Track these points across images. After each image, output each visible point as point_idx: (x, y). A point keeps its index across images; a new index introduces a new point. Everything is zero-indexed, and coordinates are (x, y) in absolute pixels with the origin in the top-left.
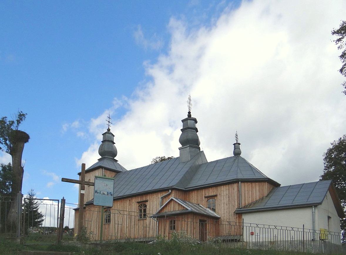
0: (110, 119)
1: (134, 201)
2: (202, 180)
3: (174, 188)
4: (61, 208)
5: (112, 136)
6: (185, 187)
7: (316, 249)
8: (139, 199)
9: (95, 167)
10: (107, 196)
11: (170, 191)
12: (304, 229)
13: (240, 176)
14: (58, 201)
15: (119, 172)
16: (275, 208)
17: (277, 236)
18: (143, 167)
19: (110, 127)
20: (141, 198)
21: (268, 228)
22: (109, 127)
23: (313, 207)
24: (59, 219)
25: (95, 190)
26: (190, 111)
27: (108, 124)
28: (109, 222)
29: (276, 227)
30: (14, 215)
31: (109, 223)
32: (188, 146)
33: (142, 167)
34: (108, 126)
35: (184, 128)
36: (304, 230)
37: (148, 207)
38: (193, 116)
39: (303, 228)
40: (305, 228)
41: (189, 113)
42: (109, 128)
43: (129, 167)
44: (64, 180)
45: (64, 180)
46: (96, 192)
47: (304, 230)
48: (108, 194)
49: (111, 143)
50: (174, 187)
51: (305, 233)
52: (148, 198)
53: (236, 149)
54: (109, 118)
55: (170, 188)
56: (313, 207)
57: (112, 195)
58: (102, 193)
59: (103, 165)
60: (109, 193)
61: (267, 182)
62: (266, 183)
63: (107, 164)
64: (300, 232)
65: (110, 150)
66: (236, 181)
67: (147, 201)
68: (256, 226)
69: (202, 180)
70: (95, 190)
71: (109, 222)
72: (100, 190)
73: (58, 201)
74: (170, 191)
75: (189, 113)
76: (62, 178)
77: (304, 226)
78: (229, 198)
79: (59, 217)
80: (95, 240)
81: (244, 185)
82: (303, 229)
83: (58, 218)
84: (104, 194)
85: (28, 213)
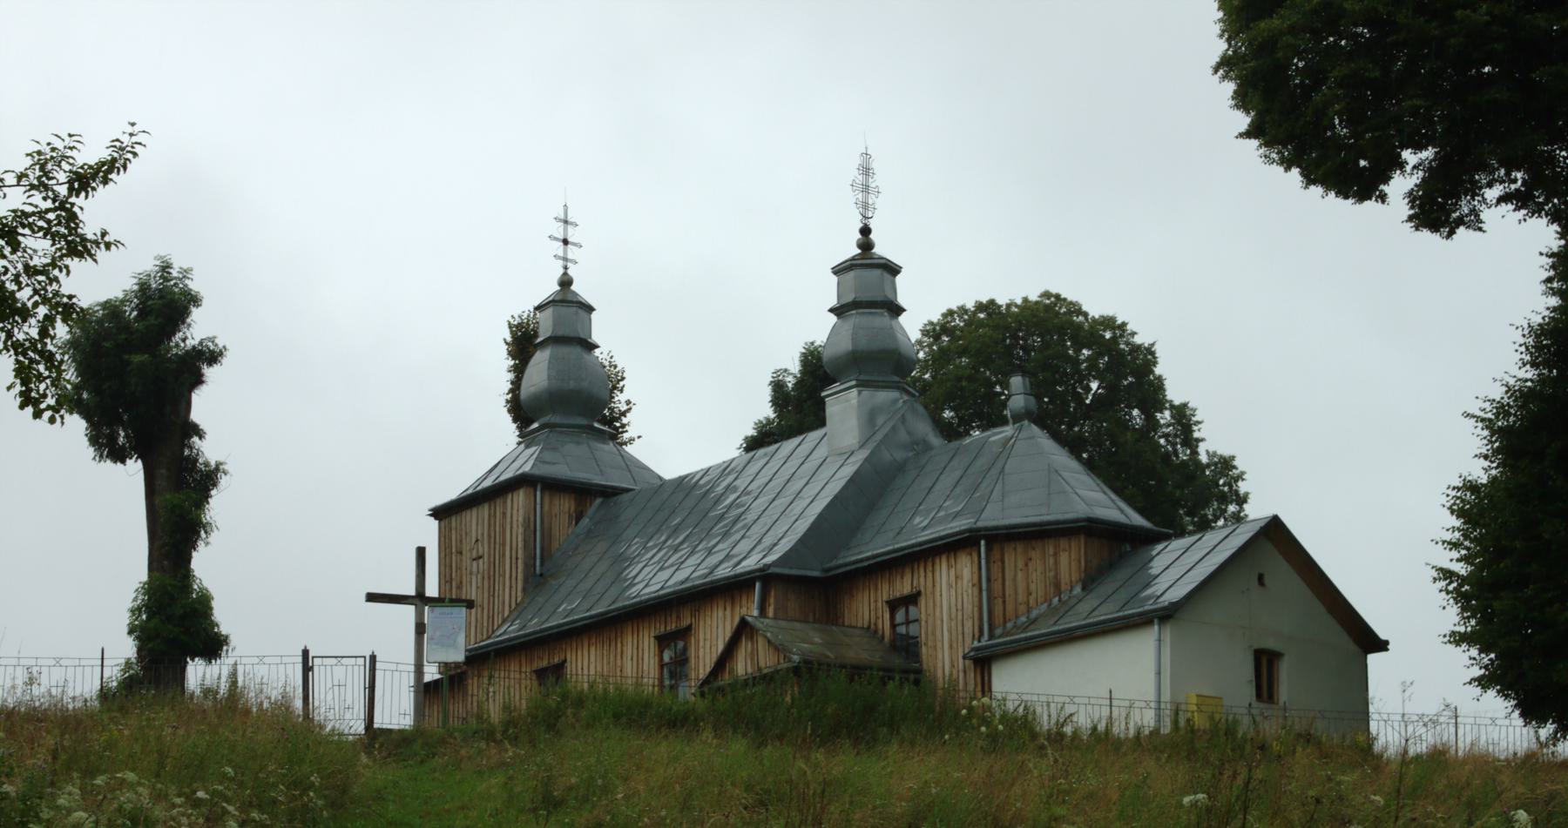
0: (561, 254)
2: (294, 691)
4: (370, 670)
5: (580, 311)
7: (512, 690)
14: (365, 657)
16: (1003, 647)
18: (709, 469)
19: (569, 265)
20: (949, 567)
22: (566, 268)
23: (1156, 621)
24: (367, 690)
26: (866, 225)
27: (561, 254)
29: (1148, 705)
32: (854, 383)
33: (680, 477)
34: (561, 263)
35: (844, 301)
36: (1111, 702)
38: (881, 249)
39: (1108, 697)
41: (865, 231)
42: (565, 274)
43: (669, 469)
44: (372, 597)
45: (372, 597)
47: (1111, 702)
49: (577, 351)
53: (1013, 397)
54: (566, 222)
55: (757, 574)
56: (1156, 621)
63: (574, 462)
65: (572, 385)
69: (294, 691)
73: (365, 657)
75: (865, 231)
77: (1111, 692)
78: (342, 688)
79: (367, 686)
83: (365, 688)
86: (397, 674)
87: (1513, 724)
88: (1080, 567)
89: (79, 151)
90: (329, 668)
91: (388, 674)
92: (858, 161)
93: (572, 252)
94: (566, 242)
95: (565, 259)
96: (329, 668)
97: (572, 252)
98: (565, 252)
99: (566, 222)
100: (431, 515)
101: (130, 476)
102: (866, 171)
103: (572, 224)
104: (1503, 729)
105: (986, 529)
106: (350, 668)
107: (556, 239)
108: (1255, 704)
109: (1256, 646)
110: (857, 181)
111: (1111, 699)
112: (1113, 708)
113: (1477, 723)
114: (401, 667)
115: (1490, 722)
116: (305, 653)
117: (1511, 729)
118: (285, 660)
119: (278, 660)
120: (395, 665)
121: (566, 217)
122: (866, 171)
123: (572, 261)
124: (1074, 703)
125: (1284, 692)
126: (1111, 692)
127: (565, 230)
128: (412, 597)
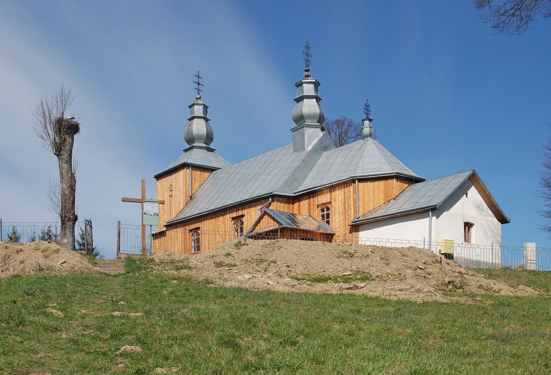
1: (229, 216)
3: (274, 194)
6: (294, 192)
8: (234, 215)
9: (171, 168)
10: (154, 216)
11: (270, 199)
12: (425, 242)
13: (360, 173)
15: (216, 170)
17: (545, 257)
21: (464, 247)
25: (144, 212)
28: (199, 250)
30: (465, 301)
31: (199, 252)
36: (424, 242)
37: (245, 224)
40: (425, 241)
44: (124, 200)
45: (124, 200)
46: (144, 214)
48: (154, 215)
50: (275, 193)
51: (494, 250)
52: (245, 212)
54: (199, 77)
57: (158, 215)
58: (149, 214)
59: (190, 161)
60: (155, 214)
61: (395, 179)
62: (394, 179)
64: (488, 250)
66: (353, 181)
67: (243, 216)
68: (386, 241)
70: (144, 212)
71: (199, 250)
72: (148, 212)
74: (270, 199)
76: (141, 179)
77: (424, 238)
80: (269, 295)
81: (282, 199)
82: (424, 241)
84: (151, 215)
85: (85, 242)
86: (466, 248)
87: (466, 247)
90: (474, 249)
94: (199, 84)
96: (474, 249)
97: (201, 88)
98: (198, 87)
99: (199, 77)
100: (154, 177)
101: (142, 203)
102: (307, 48)
103: (200, 77)
104: (482, 250)
107: (196, 83)
108: (464, 243)
109: (465, 221)
110: (304, 52)
111: (424, 241)
112: (493, 249)
113: (466, 247)
115: (387, 241)
116: (119, 222)
117: (485, 250)
118: (131, 227)
120: (531, 262)
121: (199, 75)
122: (307, 48)
123: (201, 90)
124: (479, 248)
125: (473, 240)
126: (424, 238)
127: (199, 81)
128: (141, 199)
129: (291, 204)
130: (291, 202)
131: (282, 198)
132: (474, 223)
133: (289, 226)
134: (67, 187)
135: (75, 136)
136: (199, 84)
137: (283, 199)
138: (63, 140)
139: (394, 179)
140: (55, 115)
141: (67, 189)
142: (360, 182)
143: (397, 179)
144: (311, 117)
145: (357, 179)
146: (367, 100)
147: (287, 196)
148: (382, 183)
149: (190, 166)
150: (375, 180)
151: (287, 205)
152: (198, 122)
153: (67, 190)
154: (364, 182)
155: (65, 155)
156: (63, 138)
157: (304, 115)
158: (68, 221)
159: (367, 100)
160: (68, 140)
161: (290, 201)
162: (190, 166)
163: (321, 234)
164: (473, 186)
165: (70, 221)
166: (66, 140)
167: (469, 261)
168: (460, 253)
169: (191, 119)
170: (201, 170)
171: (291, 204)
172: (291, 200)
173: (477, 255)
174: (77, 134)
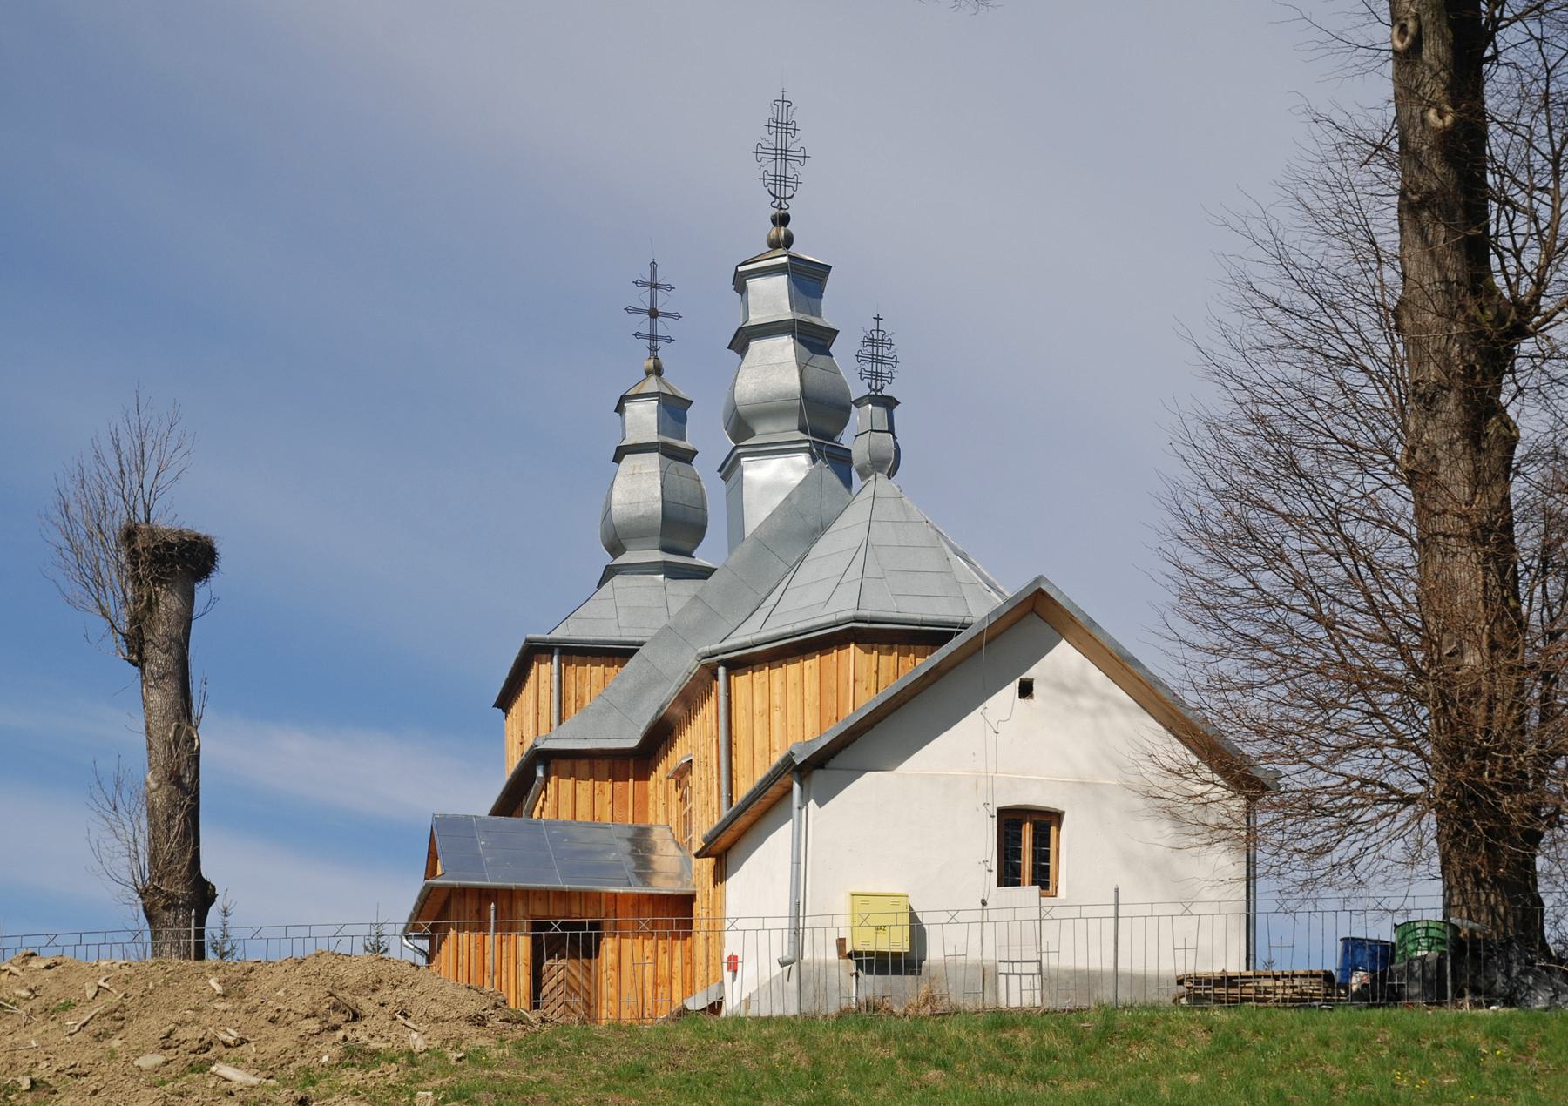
36: (1117, 909)
47: (1117, 909)
54: (654, 286)
61: (856, 643)
74: (540, 773)
77: (1117, 891)
86: (1152, 922)
88: (1161, 684)
89: (629, 310)
90: (1165, 921)
91: (1139, 922)
92: (767, 113)
93: (663, 326)
94: (654, 314)
95: (653, 337)
96: (1165, 921)
97: (663, 326)
99: (654, 286)
102: (783, 126)
105: (559, 641)
106: (1206, 920)
114: (769, 924)
117: (1152, 922)
118: (1086, 912)
119: (757, 924)
122: (783, 126)
123: (663, 339)
126: (1117, 891)
129: (631, 780)
130: (631, 774)
131: (586, 761)
132: (1060, 808)
133: (1027, 869)
134: (159, 781)
135: (202, 592)
136: (654, 314)
137: (590, 763)
138: (142, 605)
139: (852, 646)
140: (116, 522)
141: (159, 787)
142: (739, 671)
143: (866, 646)
144: (771, 411)
145: (722, 663)
146: (878, 319)
147: (602, 750)
148: (811, 664)
149: (557, 651)
150: (789, 660)
151: (608, 786)
152: (634, 467)
153: (159, 792)
154: (750, 672)
155: (158, 659)
156: (145, 598)
157: (738, 408)
158: (166, 908)
159: (878, 319)
160: (169, 602)
161: (628, 767)
162: (557, 651)
163: (619, 898)
164: (1064, 641)
165: (176, 906)
166: (158, 605)
167: (816, 967)
168: (1288, 941)
169: (620, 454)
170: (610, 659)
171: (631, 780)
172: (631, 765)
173: (1179, 944)
174: (214, 573)
